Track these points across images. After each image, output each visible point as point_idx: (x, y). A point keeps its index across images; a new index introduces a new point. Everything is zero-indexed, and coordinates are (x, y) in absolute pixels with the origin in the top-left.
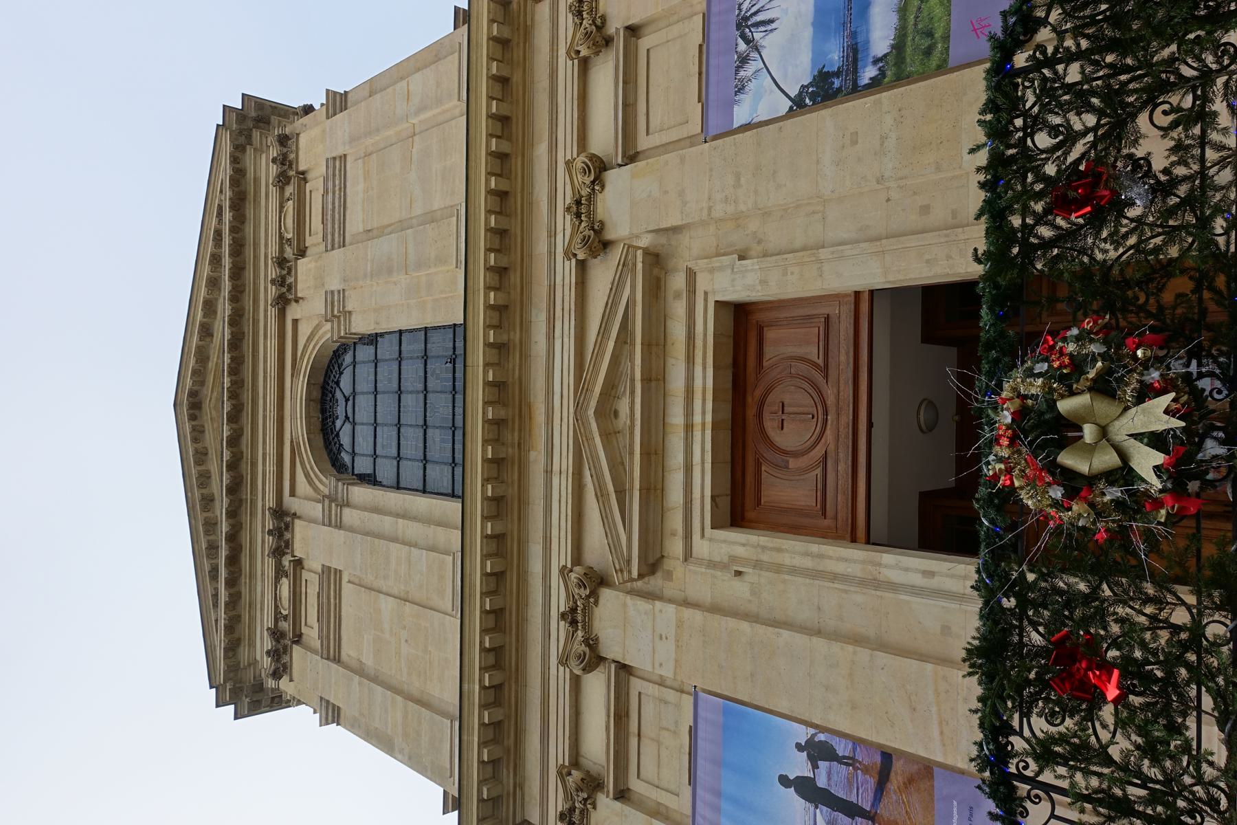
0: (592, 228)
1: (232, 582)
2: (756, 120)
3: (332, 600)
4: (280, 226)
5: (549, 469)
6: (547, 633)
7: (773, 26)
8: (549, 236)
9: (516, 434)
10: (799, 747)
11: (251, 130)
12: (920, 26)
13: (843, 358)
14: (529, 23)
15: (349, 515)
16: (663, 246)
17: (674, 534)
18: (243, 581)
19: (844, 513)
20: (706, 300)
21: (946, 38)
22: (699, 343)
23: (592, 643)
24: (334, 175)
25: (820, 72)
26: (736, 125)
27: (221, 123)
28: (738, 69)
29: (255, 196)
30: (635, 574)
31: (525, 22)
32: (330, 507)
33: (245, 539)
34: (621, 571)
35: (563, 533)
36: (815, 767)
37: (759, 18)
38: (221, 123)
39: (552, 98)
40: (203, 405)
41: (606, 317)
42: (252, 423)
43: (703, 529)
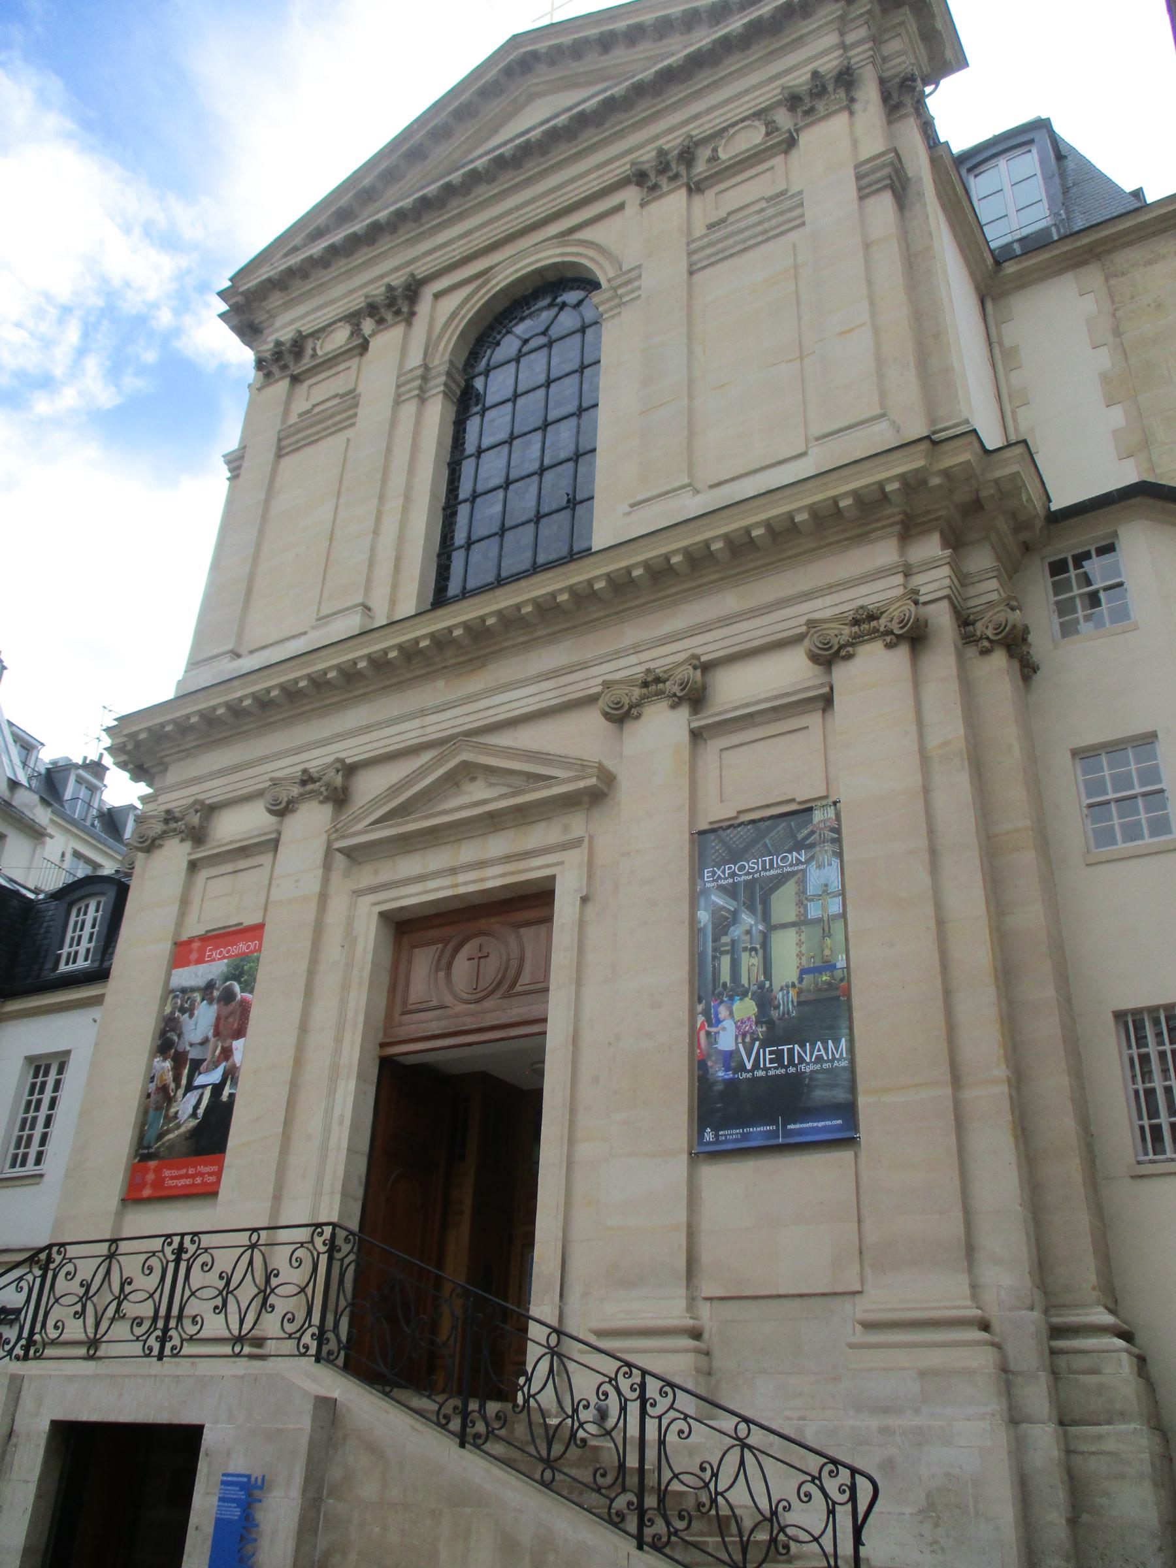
0: (631, 707)
1: (334, 252)
3: (330, 422)
4: (736, 123)
5: (426, 713)
8: (634, 646)
9: (454, 661)
13: (516, 1011)
14: (873, 536)
15: (409, 410)
17: (376, 872)
19: (402, 1033)
20: (557, 864)
22: (522, 865)
24: (782, 213)
29: (777, 50)
31: (875, 530)
32: (413, 380)
33: (385, 243)
34: (336, 831)
35: (375, 745)
39: (778, 603)
41: (538, 756)
42: (504, 191)
43: (378, 903)
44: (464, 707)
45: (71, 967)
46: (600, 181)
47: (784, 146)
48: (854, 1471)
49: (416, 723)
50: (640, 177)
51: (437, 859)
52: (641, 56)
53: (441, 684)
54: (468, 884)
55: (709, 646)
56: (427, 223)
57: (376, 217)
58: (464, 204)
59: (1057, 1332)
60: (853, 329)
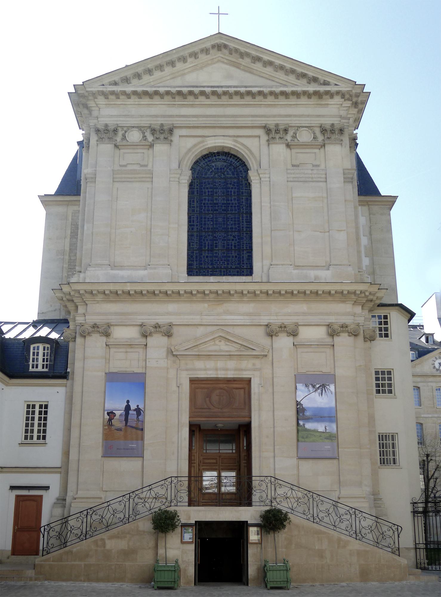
2: (297, 390)
4: (303, 127)
6: (150, 314)
7: (320, 395)
10: (138, 406)
11: (352, 101)
12: (309, 435)
16: (268, 359)
18: (136, 100)
21: (305, 441)
23: (151, 334)
25: (305, 410)
26: (297, 384)
27: (356, 83)
28: (312, 385)
30: (174, 353)
31: (347, 301)
33: (157, 100)
36: (134, 410)
37: (324, 391)
38: (356, 83)
40: (220, 52)
44: (80, 317)
45: (35, 370)
46: (252, 122)
47: (320, 147)
48: (398, 526)
49: (198, 317)
50: (268, 131)
51: (210, 364)
52: (268, 73)
53: (206, 305)
54: (221, 375)
55: (174, 319)
56: (178, 101)
57: (158, 89)
58: (195, 102)
59: (375, 500)
60: (341, 231)
